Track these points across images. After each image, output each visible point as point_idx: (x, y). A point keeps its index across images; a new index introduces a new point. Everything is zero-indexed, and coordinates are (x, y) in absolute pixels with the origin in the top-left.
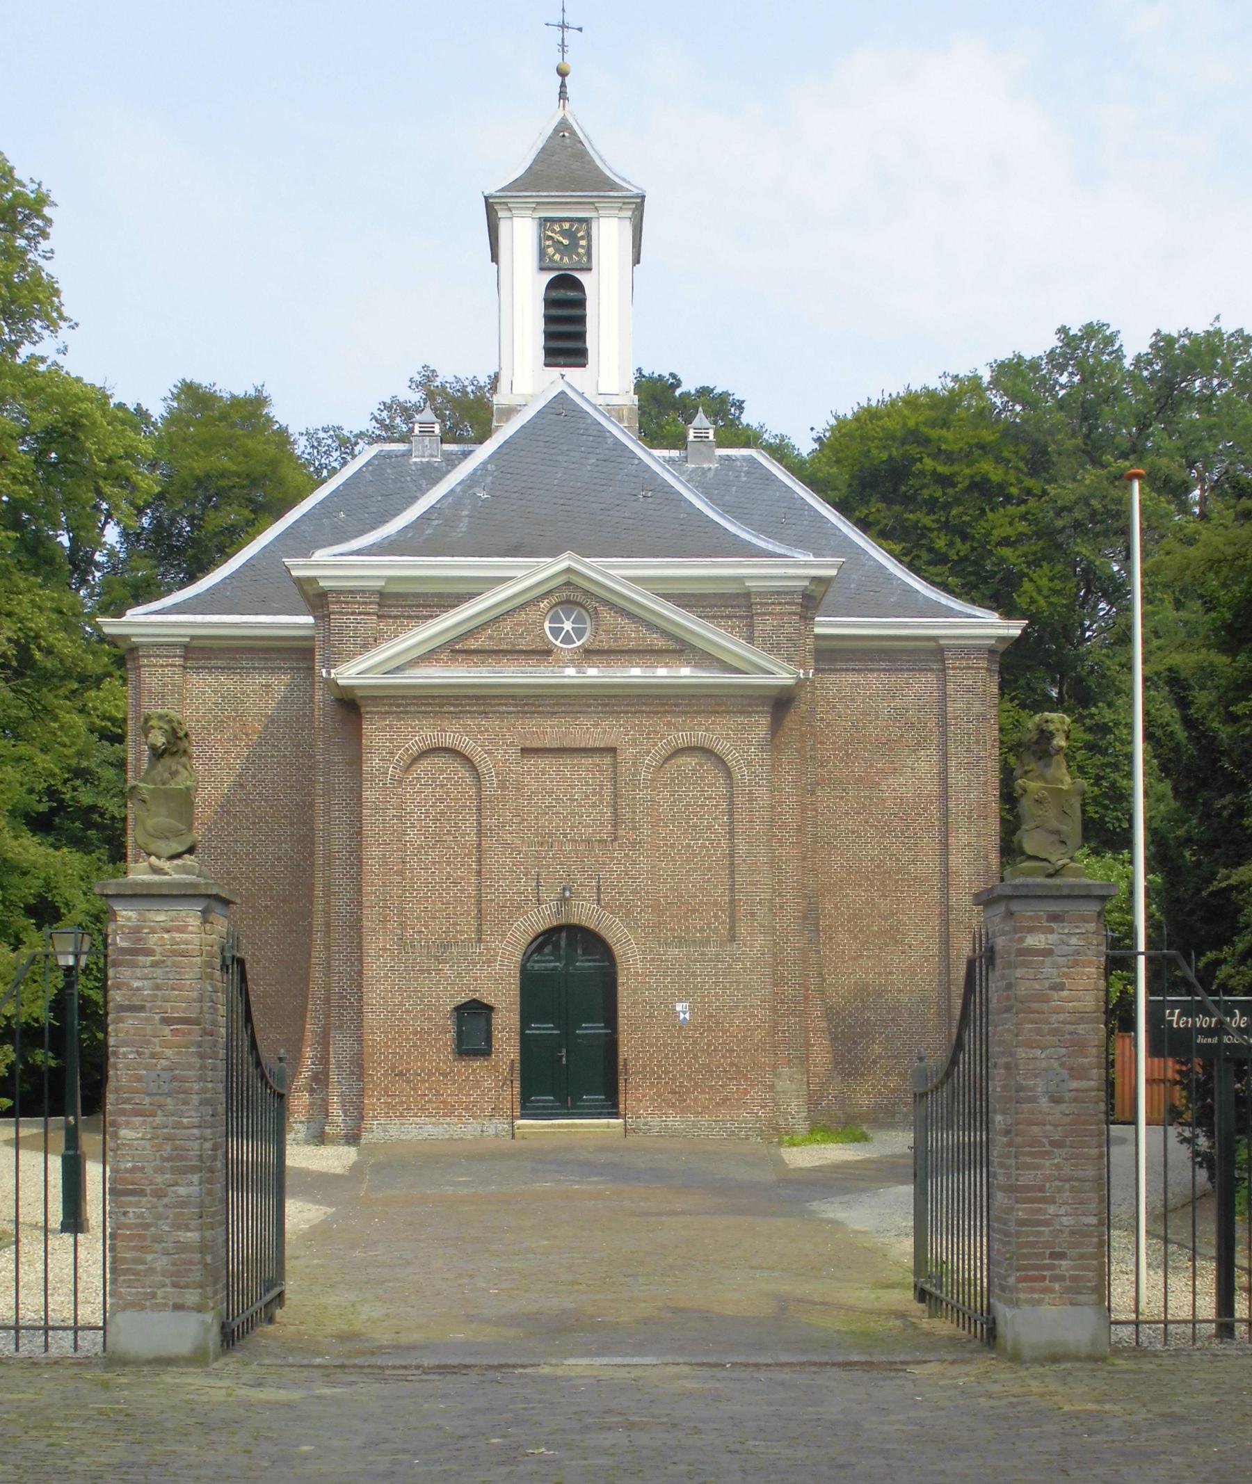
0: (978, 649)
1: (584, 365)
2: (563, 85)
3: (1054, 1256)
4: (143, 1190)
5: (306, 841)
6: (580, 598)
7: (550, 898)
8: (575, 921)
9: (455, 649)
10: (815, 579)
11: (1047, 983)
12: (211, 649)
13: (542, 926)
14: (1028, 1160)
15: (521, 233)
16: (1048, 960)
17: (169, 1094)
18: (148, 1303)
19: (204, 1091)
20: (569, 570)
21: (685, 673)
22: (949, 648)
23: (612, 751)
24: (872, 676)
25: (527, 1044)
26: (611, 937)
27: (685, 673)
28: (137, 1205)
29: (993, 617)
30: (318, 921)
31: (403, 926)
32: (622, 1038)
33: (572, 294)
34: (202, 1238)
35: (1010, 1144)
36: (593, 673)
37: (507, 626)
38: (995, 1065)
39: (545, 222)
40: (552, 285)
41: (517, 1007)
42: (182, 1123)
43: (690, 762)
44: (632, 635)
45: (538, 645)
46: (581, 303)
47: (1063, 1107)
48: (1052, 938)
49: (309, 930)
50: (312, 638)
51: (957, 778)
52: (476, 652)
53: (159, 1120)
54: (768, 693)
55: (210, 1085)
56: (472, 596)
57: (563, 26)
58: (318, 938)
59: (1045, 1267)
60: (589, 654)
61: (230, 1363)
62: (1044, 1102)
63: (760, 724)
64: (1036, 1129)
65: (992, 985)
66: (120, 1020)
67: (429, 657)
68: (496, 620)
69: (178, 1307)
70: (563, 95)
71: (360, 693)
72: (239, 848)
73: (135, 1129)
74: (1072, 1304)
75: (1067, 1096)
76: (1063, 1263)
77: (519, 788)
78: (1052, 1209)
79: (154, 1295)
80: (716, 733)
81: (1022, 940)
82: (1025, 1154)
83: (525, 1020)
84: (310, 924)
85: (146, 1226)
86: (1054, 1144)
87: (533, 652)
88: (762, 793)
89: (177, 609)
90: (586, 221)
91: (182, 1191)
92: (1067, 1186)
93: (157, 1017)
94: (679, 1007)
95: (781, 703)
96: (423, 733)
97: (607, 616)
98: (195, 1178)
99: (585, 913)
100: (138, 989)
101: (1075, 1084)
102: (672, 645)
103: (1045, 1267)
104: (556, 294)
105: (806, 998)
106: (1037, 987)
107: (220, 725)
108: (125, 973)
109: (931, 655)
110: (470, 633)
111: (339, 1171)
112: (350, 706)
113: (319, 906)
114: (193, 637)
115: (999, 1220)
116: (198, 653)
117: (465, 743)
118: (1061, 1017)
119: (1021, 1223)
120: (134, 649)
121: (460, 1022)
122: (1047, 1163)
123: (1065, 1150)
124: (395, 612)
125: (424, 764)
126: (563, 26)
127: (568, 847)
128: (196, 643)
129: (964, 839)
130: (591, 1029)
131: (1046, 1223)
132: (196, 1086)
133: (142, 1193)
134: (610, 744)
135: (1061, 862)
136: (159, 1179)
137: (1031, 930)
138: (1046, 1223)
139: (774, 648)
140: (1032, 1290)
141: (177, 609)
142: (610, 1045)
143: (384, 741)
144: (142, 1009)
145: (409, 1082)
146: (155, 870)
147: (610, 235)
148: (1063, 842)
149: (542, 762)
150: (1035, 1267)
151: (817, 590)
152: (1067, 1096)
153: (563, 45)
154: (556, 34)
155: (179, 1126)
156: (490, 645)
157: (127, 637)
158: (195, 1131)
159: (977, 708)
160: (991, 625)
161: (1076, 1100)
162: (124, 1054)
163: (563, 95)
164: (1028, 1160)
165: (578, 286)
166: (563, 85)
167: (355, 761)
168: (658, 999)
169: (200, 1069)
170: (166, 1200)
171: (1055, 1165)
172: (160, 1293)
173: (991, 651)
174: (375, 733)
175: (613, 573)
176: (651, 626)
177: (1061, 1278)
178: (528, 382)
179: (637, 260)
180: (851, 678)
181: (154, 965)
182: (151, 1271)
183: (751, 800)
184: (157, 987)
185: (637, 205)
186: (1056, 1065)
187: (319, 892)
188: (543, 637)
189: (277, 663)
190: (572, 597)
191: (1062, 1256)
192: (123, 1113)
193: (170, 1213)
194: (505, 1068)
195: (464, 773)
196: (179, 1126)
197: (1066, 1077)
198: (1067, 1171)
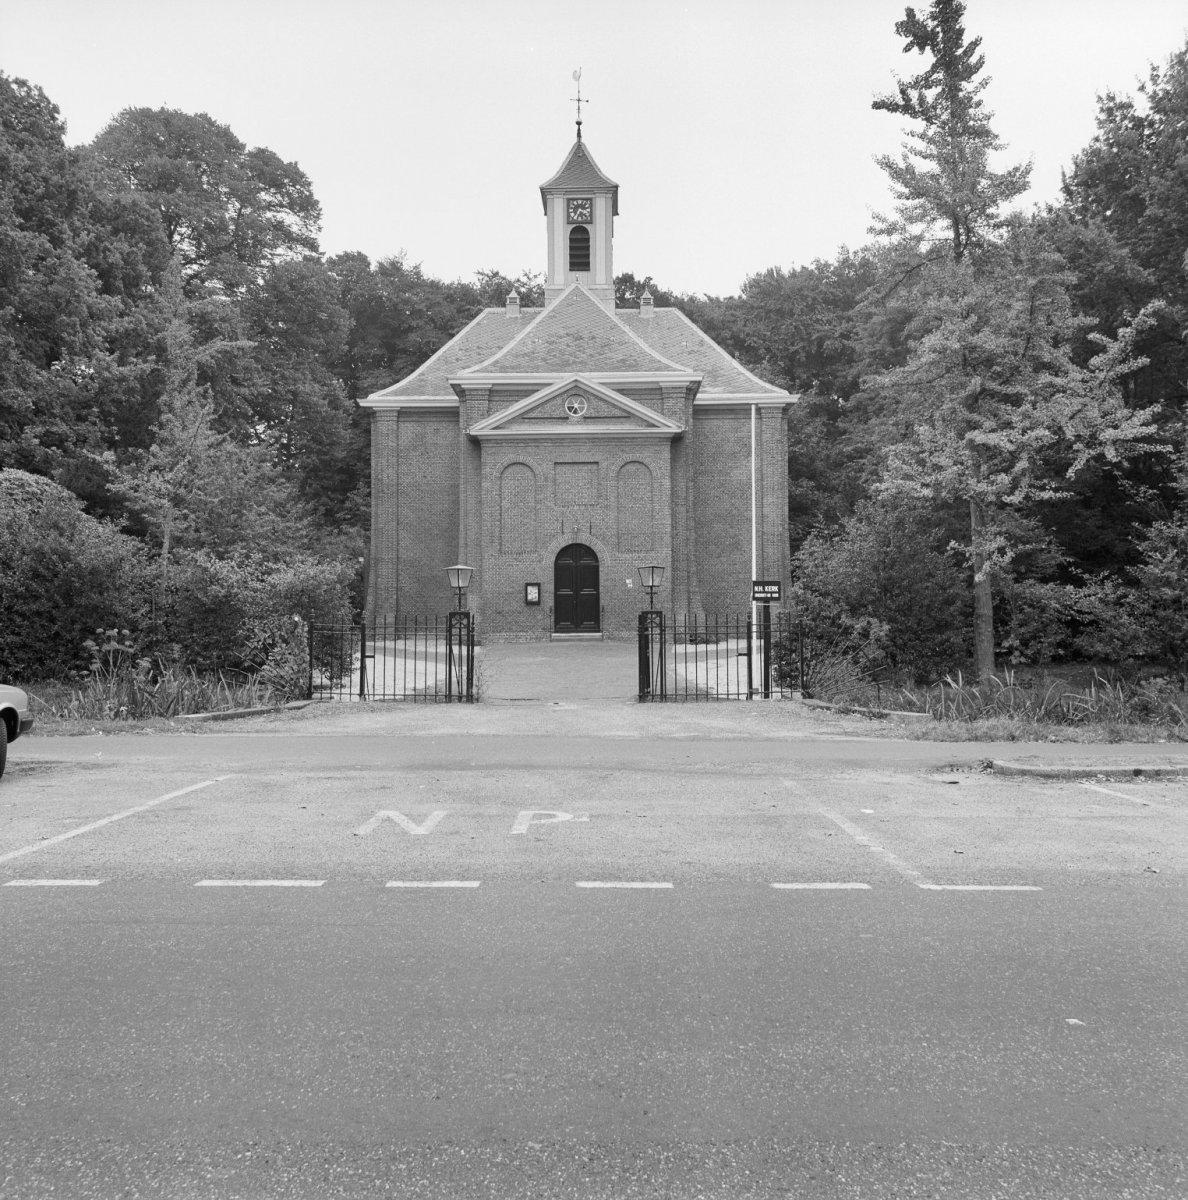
0: (778, 408)
1: (589, 270)
2: (579, 130)
5: (456, 502)
6: (581, 393)
8: (579, 542)
9: (523, 417)
13: (564, 545)
15: (559, 204)
20: (576, 381)
22: (763, 408)
23: (597, 463)
24: (726, 421)
25: (557, 598)
26: (595, 549)
30: (462, 542)
31: (500, 544)
32: (602, 595)
39: (569, 200)
41: (553, 581)
43: (632, 468)
44: (605, 410)
45: (562, 415)
46: (587, 240)
49: (457, 546)
50: (458, 407)
52: (534, 418)
54: (668, 436)
56: (654, 426)
57: (579, 100)
58: (462, 550)
63: (667, 449)
68: (542, 404)
72: (423, 506)
80: (645, 455)
83: (557, 589)
84: (458, 543)
87: (560, 418)
88: (667, 483)
89: (395, 393)
90: (591, 199)
94: (627, 581)
95: (676, 440)
96: (510, 456)
97: (595, 402)
99: (584, 538)
102: (625, 414)
105: (688, 577)
107: (415, 448)
110: (532, 410)
112: (476, 442)
113: (462, 535)
116: (403, 413)
117: (530, 461)
120: (375, 412)
124: (497, 398)
125: (510, 470)
127: (576, 508)
129: (771, 500)
134: (596, 460)
141: (395, 393)
142: (597, 598)
143: (493, 461)
147: (601, 204)
149: (564, 468)
156: (540, 415)
157: (371, 408)
159: (778, 437)
165: (585, 231)
166: (579, 130)
167: (479, 468)
174: (487, 456)
175: (592, 379)
176: (614, 406)
178: (564, 279)
179: (615, 213)
180: (715, 422)
183: (661, 486)
187: (461, 527)
189: (442, 419)
195: (525, 469)
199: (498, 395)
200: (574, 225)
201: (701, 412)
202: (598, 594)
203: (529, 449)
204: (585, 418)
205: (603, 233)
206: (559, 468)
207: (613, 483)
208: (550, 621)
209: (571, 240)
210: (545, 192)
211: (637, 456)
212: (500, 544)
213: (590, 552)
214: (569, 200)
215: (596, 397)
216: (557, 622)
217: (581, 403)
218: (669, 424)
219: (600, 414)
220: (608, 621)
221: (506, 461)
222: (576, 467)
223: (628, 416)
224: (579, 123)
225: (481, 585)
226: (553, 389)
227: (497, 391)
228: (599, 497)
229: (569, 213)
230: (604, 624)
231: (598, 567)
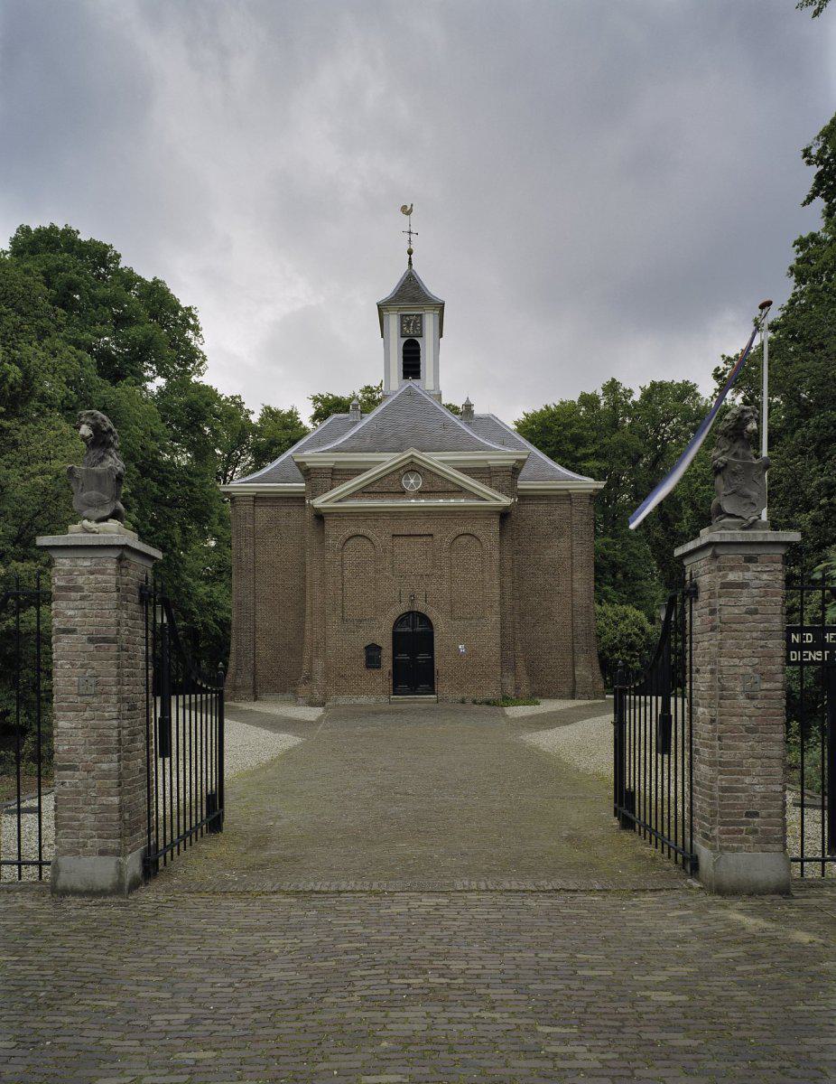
2: (410, 259)
3: (748, 814)
4: (76, 766)
7: (405, 599)
9: (364, 492)
10: (518, 460)
11: (744, 609)
12: (265, 498)
14: (730, 742)
15: (393, 322)
16: (745, 591)
17: (95, 695)
18: (81, 850)
19: (119, 692)
20: (412, 456)
21: (462, 502)
23: (432, 535)
25: (396, 664)
27: (462, 502)
28: (73, 777)
29: (591, 480)
31: (343, 612)
33: (413, 348)
34: (121, 801)
35: (714, 731)
36: (422, 502)
37: (386, 481)
38: (698, 671)
39: (402, 316)
40: (405, 344)
42: (104, 716)
43: (463, 540)
44: (439, 485)
45: (399, 489)
46: (418, 351)
47: (755, 702)
48: (749, 575)
51: (577, 550)
53: (87, 714)
55: (126, 688)
57: (410, 233)
59: (743, 823)
60: (422, 493)
61: (154, 884)
62: (742, 700)
63: (496, 521)
64: (735, 719)
65: (695, 613)
66: (58, 640)
67: (353, 496)
69: (102, 853)
70: (410, 263)
71: (323, 511)
73: (70, 721)
74: (762, 851)
75: (760, 694)
76: (757, 820)
77: (392, 552)
78: (748, 780)
79: (85, 845)
81: (725, 576)
82: (727, 738)
85: (79, 793)
86: (749, 730)
88: (496, 555)
90: (421, 315)
91: (105, 766)
92: (759, 762)
93: (85, 637)
95: (504, 515)
98: (115, 757)
99: (420, 606)
100: (71, 617)
101: (765, 686)
102: (456, 489)
103: (743, 823)
104: (408, 348)
106: (736, 611)
108: (63, 604)
109: (567, 497)
111: (313, 720)
112: (320, 517)
114: (257, 493)
115: (698, 783)
116: (258, 499)
117: (369, 532)
118: (755, 635)
119: (724, 790)
121: (367, 653)
122: (743, 745)
123: (758, 735)
124: (338, 477)
125: (352, 542)
126: (410, 233)
128: (259, 495)
129: (580, 575)
130: (404, 657)
131: (743, 790)
132: (114, 689)
133: (74, 768)
135: (753, 518)
136: (88, 757)
137: (732, 569)
138: (743, 790)
139: (501, 491)
140: (732, 840)
142: (432, 662)
143: (335, 533)
144: (73, 631)
145: (345, 679)
146: (86, 530)
147: (429, 322)
148: (754, 504)
150: (733, 823)
151: (519, 466)
152: (760, 694)
153: (410, 241)
154: (407, 235)
155: (102, 718)
157: (230, 492)
158: (115, 722)
160: (589, 484)
161: (766, 697)
162: (61, 665)
163: (410, 263)
164: (730, 742)
165: (418, 345)
166: (410, 259)
168: (451, 644)
169: (118, 676)
170: (93, 774)
171: (750, 746)
172: (90, 842)
173: (591, 495)
175: (433, 459)
176: (448, 481)
177: (755, 832)
179: (441, 336)
181: (82, 598)
182: (81, 827)
184: (85, 616)
185: (441, 307)
186: (750, 670)
188: (401, 486)
190: (412, 468)
191: (756, 814)
192: (61, 709)
193: (98, 783)
194: (386, 674)
196: (102, 718)
197: (758, 679)
198: (759, 750)
199: (337, 474)
200: (407, 339)
201: (525, 497)
202: (433, 659)
203: (369, 522)
204: (420, 492)
205: (432, 336)
206: (397, 540)
207: (447, 554)
208: (389, 684)
209: (405, 352)
210: (382, 308)
211: (469, 529)
212: (343, 612)
213: (424, 619)
214: (402, 316)
215: (431, 472)
216: (395, 685)
217: (416, 479)
218: (498, 497)
219: (435, 489)
220: (443, 686)
221: (347, 533)
222: (412, 539)
223: (460, 491)
224: (410, 252)
225: (325, 650)
226: (384, 467)
227: (339, 470)
228: (434, 567)
229: (402, 328)
230: (438, 687)
231: (433, 632)
